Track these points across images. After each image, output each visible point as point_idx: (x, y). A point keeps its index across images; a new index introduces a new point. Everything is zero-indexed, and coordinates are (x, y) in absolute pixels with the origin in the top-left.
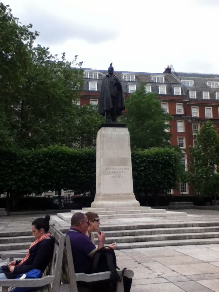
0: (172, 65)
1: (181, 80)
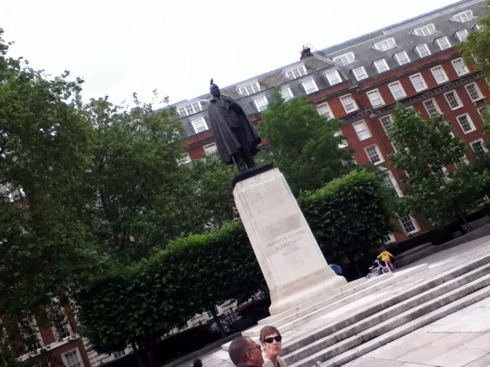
1: (332, 59)
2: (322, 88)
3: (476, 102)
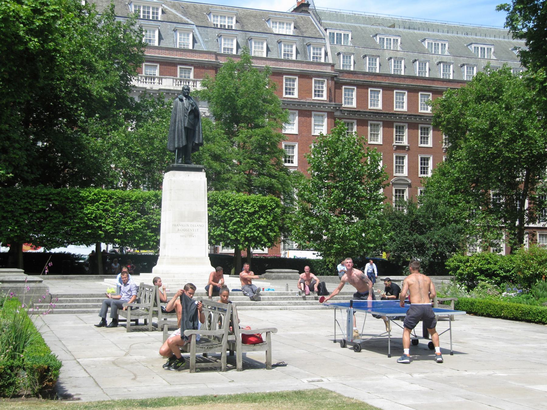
3: (397, 146)
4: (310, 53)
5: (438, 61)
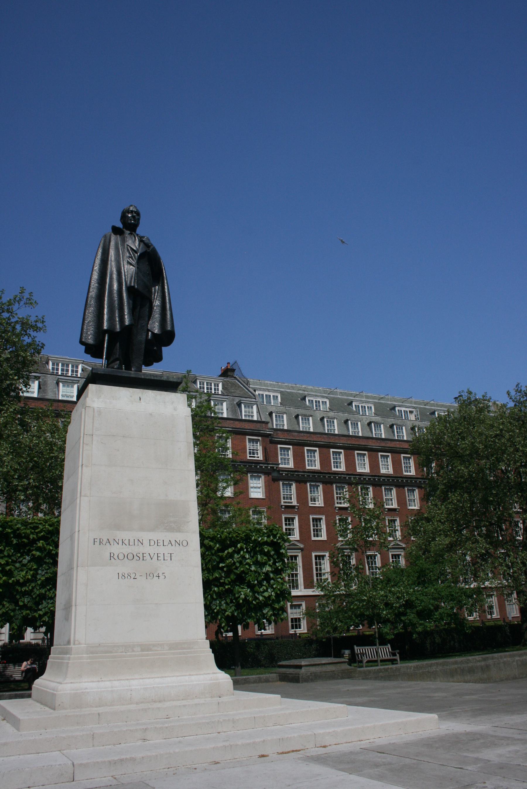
0: (236, 362)
1: (255, 391)
2: (230, 417)
4: (241, 412)
5: (368, 421)
